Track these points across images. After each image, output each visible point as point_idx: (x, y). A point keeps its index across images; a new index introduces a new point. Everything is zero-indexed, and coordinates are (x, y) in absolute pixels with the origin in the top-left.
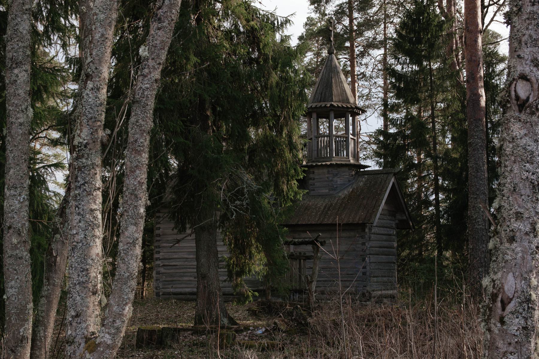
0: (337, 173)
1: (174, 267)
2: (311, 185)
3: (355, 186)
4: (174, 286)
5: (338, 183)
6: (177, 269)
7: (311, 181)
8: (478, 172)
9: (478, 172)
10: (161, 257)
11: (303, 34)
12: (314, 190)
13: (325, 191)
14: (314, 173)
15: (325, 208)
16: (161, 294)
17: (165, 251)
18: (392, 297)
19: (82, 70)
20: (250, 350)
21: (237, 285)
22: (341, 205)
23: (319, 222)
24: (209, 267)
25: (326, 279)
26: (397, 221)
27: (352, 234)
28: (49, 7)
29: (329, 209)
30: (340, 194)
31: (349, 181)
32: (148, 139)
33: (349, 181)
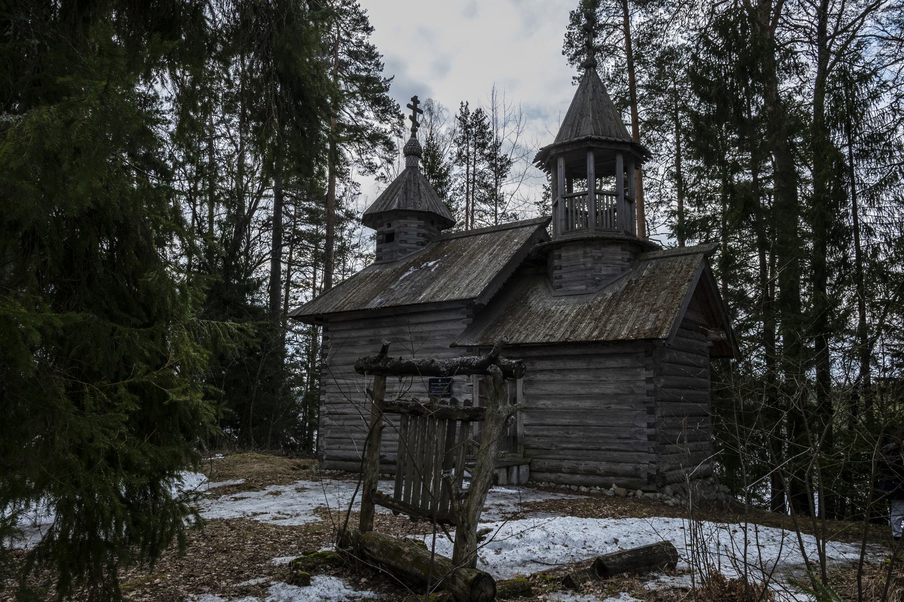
0: (600, 255)
1: (342, 417)
2: (556, 278)
4: (342, 446)
5: (603, 272)
6: (346, 419)
7: (556, 272)
10: (327, 400)
12: (561, 287)
14: (560, 257)
16: (324, 457)
20: (37, 500)
21: (212, 423)
25: (579, 445)
26: (710, 343)
27: (627, 362)
31: (623, 270)
32: (574, 253)
33: (623, 270)
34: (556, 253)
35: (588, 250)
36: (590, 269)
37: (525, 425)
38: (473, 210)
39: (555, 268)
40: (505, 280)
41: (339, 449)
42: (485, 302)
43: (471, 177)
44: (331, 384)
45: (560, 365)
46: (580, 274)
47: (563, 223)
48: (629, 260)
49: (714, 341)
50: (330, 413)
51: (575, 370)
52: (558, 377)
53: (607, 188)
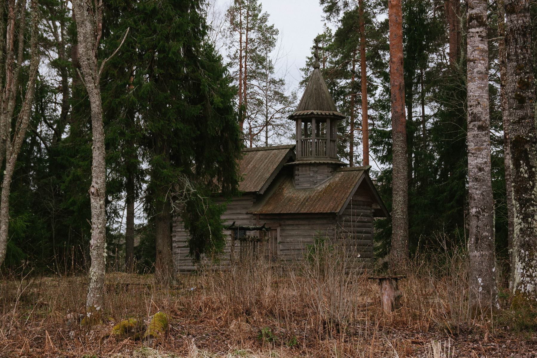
3: (332, 181)
8: (398, 173)
9: (398, 173)
10: (177, 240)
11: (306, 62)
12: (298, 185)
13: (307, 185)
14: (298, 170)
15: (304, 200)
17: (179, 234)
18: (161, 260)
19: (12, 123)
22: (317, 197)
23: (297, 212)
24: (164, 246)
26: (373, 211)
27: (325, 221)
28: (38, 77)
29: (307, 201)
30: (319, 188)
34: (297, 168)
35: (311, 168)
36: (312, 177)
37: (281, 250)
38: (246, 95)
39: (296, 175)
40: (274, 178)
41: (185, 265)
42: (262, 193)
43: (244, 45)
44: (179, 232)
45: (297, 222)
46: (307, 179)
47: (300, 152)
48: (331, 172)
49: (375, 210)
50: (179, 247)
51: (303, 225)
52: (296, 228)
53: (357, 66)
